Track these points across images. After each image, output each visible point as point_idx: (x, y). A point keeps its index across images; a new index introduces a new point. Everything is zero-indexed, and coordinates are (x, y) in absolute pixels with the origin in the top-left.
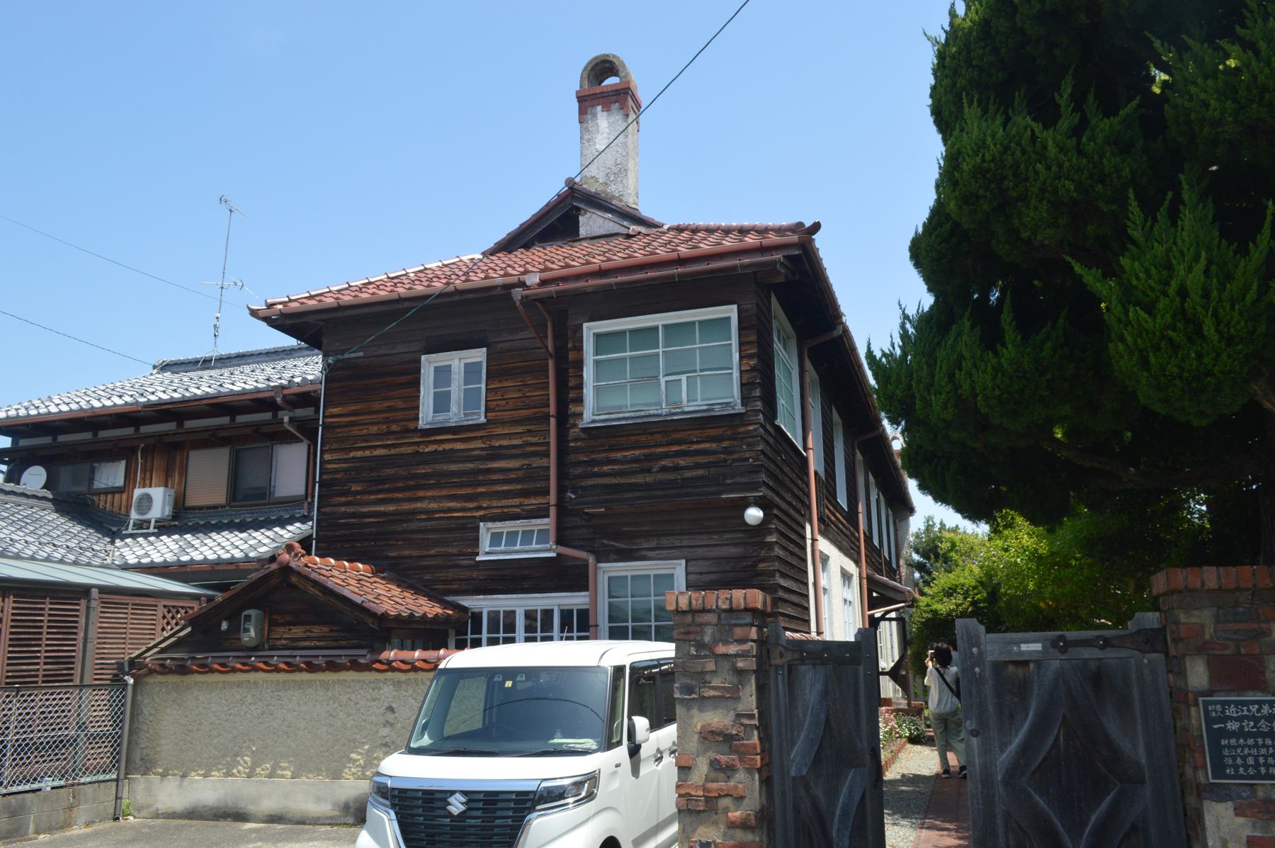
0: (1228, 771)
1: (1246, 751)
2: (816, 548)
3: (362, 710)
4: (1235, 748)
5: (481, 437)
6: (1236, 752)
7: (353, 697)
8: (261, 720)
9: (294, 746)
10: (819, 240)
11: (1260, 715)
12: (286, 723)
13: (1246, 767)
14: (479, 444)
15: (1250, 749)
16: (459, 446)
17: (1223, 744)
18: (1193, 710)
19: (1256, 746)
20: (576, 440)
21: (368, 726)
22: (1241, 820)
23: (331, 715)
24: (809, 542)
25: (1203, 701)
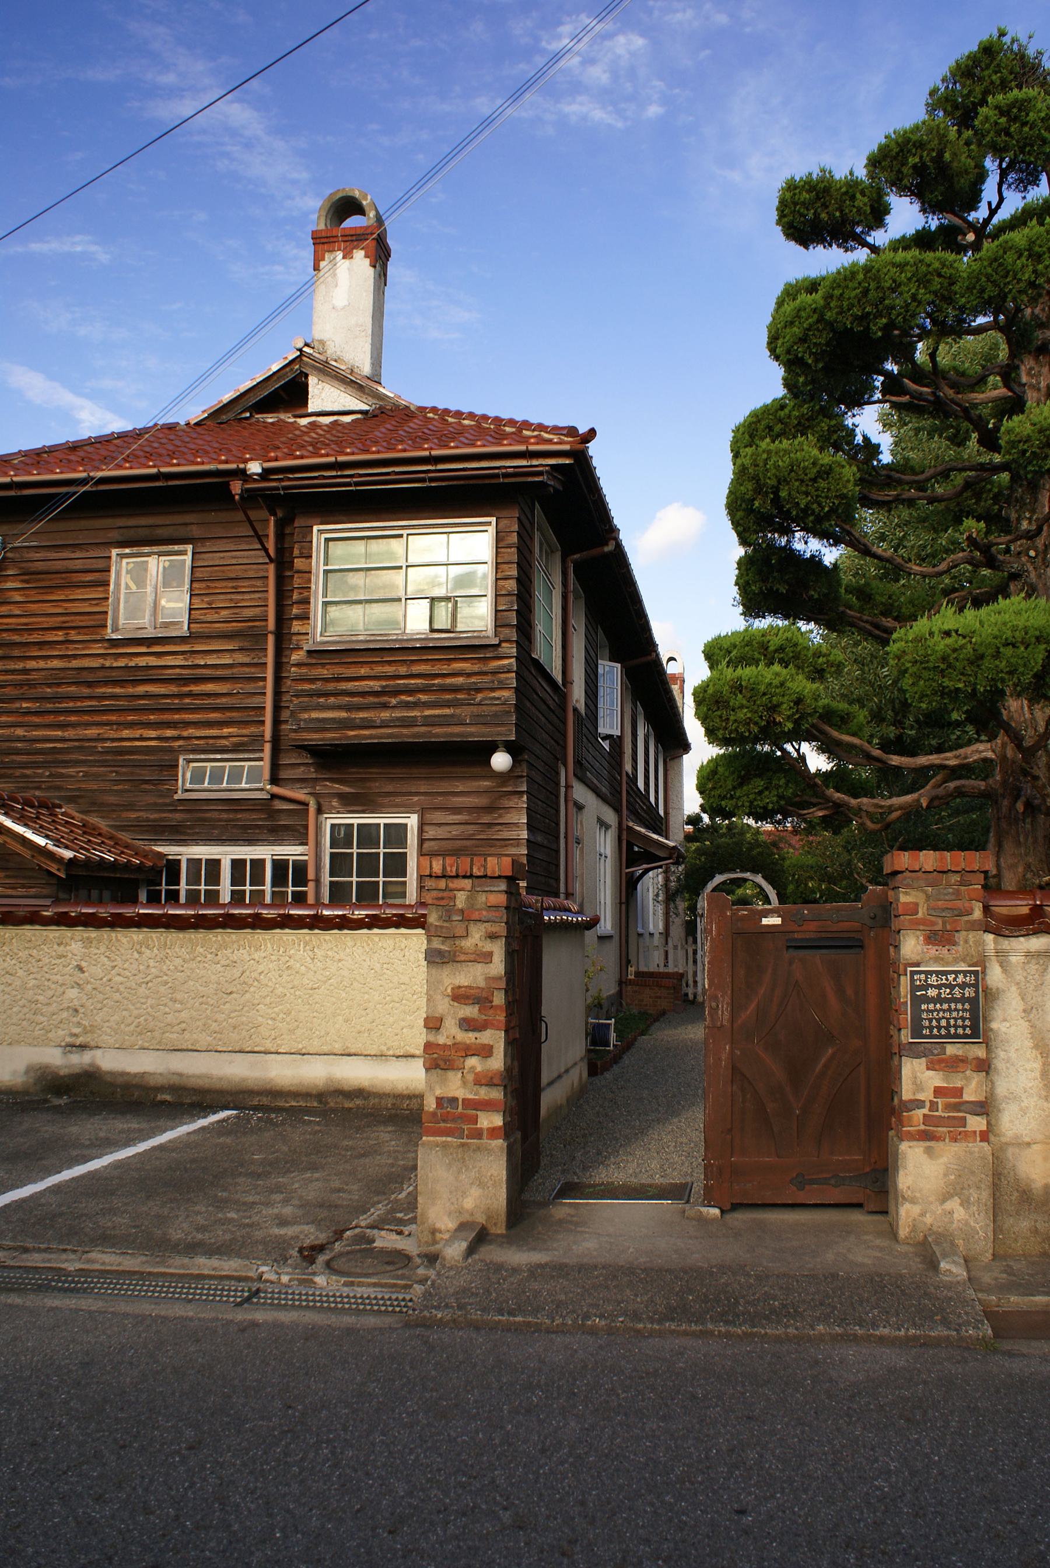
2: (569, 795)
3: (45, 969)
4: (932, 1011)
5: (183, 653)
7: (34, 952)
10: (593, 448)
13: (939, 1028)
14: (179, 661)
16: (153, 661)
18: (902, 978)
19: (950, 1010)
20: (299, 665)
21: (53, 986)
22: (931, 1073)
23: (7, 973)
24: (563, 790)
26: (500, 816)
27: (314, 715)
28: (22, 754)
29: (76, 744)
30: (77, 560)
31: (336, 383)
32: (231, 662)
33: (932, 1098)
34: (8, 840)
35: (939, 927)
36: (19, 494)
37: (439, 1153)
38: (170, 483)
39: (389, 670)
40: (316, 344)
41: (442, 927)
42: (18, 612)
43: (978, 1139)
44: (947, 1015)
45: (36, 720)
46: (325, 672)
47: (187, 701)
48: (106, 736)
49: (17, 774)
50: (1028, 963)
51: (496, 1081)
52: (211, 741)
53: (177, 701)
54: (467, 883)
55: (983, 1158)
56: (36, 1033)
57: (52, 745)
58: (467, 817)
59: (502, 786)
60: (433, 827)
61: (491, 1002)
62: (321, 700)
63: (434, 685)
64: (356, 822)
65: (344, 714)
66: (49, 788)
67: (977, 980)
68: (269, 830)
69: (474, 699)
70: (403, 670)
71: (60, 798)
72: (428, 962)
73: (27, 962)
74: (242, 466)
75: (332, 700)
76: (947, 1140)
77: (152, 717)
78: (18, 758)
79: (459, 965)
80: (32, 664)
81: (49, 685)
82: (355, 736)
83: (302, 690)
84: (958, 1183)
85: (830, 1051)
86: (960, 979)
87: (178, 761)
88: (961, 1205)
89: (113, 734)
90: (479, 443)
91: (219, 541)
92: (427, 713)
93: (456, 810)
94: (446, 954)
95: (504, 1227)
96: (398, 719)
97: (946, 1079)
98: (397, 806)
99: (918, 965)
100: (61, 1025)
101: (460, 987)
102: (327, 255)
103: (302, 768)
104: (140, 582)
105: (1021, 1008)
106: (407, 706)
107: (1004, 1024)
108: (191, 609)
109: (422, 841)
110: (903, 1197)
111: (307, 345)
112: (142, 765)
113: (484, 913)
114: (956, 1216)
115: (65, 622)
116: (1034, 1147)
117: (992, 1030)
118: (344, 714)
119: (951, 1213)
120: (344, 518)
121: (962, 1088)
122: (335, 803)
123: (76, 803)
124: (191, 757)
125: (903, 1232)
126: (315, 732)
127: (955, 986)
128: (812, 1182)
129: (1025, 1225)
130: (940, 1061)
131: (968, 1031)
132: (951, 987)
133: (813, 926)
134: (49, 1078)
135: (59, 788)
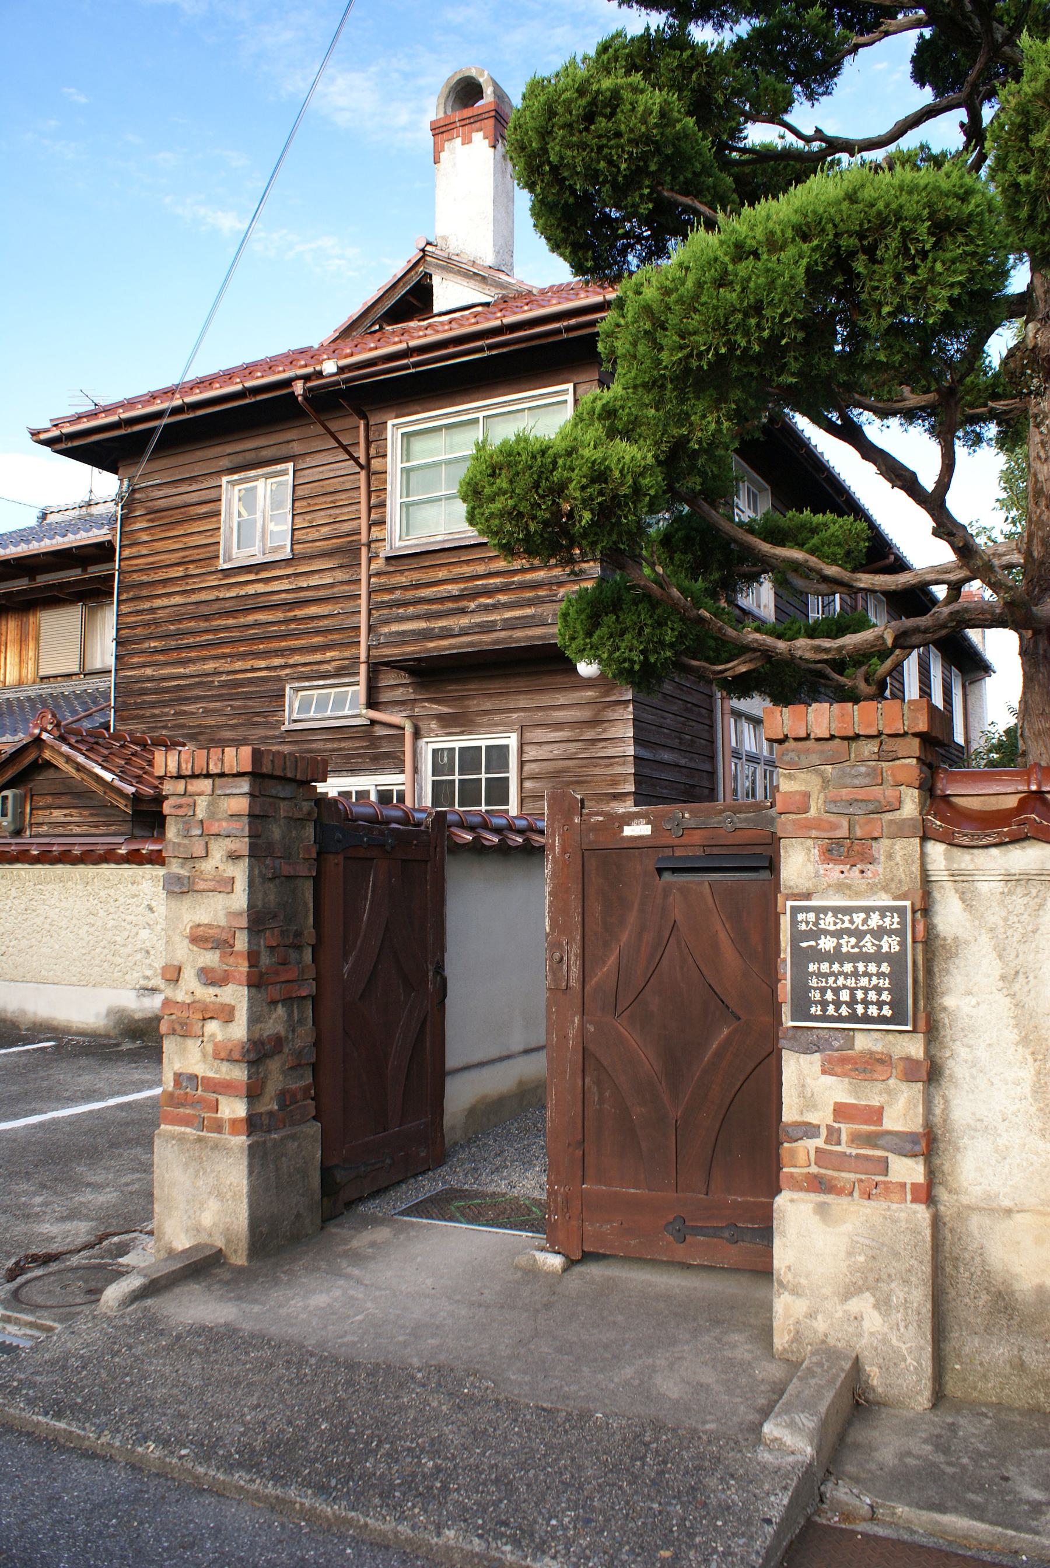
0: (813, 1010)
1: (841, 981)
3: (121, 909)
4: (826, 976)
5: (288, 576)
6: (827, 983)
7: (112, 892)
8: (25, 917)
9: (57, 947)
11: (865, 927)
12: (49, 921)
13: (838, 1004)
14: (285, 585)
15: (846, 979)
16: (261, 588)
17: (811, 970)
19: (855, 974)
21: (128, 927)
23: (90, 913)
25: (792, 907)
26: (605, 731)
27: (395, 628)
28: (151, 694)
29: (197, 680)
30: (191, 493)
31: (459, 279)
32: (331, 581)
33: (830, 1122)
34: (85, 777)
35: (843, 832)
36: (129, 431)
37: (176, 1148)
38: (259, 398)
39: (467, 570)
40: (440, 242)
41: (179, 844)
42: (146, 552)
43: (909, 1197)
44: (851, 982)
45: (161, 658)
46: (403, 579)
47: (293, 626)
48: (221, 669)
49: (148, 714)
50: (1010, 893)
51: (236, 1055)
52: (315, 668)
53: (283, 628)
54: (206, 785)
55: (915, 1232)
56: (116, 974)
57: (176, 683)
58: (569, 734)
59: (605, 697)
60: (534, 747)
61: (232, 946)
62: (401, 611)
63: (513, 583)
64: (457, 745)
65: (422, 625)
66: (174, 727)
67: (903, 922)
68: (371, 759)
69: (555, 595)
70: (481, 569)
71: (183, 736)
72: (168, 892)
73: (107, 902)
74: (318, 368)
75: (411, 610)
76: (856, 1194)
77: (261, 646)
78: (146, 698)
79: (199, 895)
80: (158, 603)
81: (172, 622)
82: (434, 647)
83: (382, 602)
84: (871, 1270)
85: (726, 1031)
86: (875, 921)
87: (284, 690)
88: (876, 1306)
89: (228, 667)
90: (554, 302)
91: (318, 456)
92: (508, 615)
93: (557, 726)
94: (186, 881)
95: (245, 1258)
96: (478, 625)
97: (855, 1092)
98: (496, 725)
99: (808, 896)
100: (135, 967)
101: (199, 925)
102: (447, 145)
103: (401, 690)
104: (251, 507)
105: (998, 972)
106: (486, 608)
107: (968, 999)
108: (293, 530)
109: (522, 763)
110: (781, 1284)
111: (429, 244)
112: (250, 696)
113: (224, 824)
114: (866, 1324)
115: (184, 557)
116: (1018, 1217)
117: (945, 1009)
118: (422, 625)
119: (858, 1318)
120: (419, 409)
121: (881, 1109)
122: (434, 725)
123: (197, 740)
124: (297, 685)
125: (781, 1340)
126: (395, 646)
127: (866, 932)
128: (697, 1231)
129: (1000, 1352)
130: (843, 1061)
131: (887, 1011)
132: (859, 935)
133: (697, 837)
134: (126, 1021)
135: (182, 726)
